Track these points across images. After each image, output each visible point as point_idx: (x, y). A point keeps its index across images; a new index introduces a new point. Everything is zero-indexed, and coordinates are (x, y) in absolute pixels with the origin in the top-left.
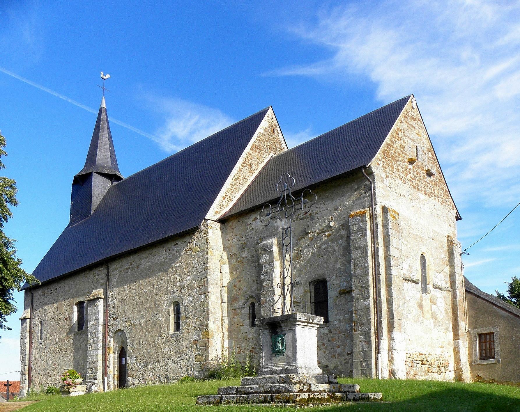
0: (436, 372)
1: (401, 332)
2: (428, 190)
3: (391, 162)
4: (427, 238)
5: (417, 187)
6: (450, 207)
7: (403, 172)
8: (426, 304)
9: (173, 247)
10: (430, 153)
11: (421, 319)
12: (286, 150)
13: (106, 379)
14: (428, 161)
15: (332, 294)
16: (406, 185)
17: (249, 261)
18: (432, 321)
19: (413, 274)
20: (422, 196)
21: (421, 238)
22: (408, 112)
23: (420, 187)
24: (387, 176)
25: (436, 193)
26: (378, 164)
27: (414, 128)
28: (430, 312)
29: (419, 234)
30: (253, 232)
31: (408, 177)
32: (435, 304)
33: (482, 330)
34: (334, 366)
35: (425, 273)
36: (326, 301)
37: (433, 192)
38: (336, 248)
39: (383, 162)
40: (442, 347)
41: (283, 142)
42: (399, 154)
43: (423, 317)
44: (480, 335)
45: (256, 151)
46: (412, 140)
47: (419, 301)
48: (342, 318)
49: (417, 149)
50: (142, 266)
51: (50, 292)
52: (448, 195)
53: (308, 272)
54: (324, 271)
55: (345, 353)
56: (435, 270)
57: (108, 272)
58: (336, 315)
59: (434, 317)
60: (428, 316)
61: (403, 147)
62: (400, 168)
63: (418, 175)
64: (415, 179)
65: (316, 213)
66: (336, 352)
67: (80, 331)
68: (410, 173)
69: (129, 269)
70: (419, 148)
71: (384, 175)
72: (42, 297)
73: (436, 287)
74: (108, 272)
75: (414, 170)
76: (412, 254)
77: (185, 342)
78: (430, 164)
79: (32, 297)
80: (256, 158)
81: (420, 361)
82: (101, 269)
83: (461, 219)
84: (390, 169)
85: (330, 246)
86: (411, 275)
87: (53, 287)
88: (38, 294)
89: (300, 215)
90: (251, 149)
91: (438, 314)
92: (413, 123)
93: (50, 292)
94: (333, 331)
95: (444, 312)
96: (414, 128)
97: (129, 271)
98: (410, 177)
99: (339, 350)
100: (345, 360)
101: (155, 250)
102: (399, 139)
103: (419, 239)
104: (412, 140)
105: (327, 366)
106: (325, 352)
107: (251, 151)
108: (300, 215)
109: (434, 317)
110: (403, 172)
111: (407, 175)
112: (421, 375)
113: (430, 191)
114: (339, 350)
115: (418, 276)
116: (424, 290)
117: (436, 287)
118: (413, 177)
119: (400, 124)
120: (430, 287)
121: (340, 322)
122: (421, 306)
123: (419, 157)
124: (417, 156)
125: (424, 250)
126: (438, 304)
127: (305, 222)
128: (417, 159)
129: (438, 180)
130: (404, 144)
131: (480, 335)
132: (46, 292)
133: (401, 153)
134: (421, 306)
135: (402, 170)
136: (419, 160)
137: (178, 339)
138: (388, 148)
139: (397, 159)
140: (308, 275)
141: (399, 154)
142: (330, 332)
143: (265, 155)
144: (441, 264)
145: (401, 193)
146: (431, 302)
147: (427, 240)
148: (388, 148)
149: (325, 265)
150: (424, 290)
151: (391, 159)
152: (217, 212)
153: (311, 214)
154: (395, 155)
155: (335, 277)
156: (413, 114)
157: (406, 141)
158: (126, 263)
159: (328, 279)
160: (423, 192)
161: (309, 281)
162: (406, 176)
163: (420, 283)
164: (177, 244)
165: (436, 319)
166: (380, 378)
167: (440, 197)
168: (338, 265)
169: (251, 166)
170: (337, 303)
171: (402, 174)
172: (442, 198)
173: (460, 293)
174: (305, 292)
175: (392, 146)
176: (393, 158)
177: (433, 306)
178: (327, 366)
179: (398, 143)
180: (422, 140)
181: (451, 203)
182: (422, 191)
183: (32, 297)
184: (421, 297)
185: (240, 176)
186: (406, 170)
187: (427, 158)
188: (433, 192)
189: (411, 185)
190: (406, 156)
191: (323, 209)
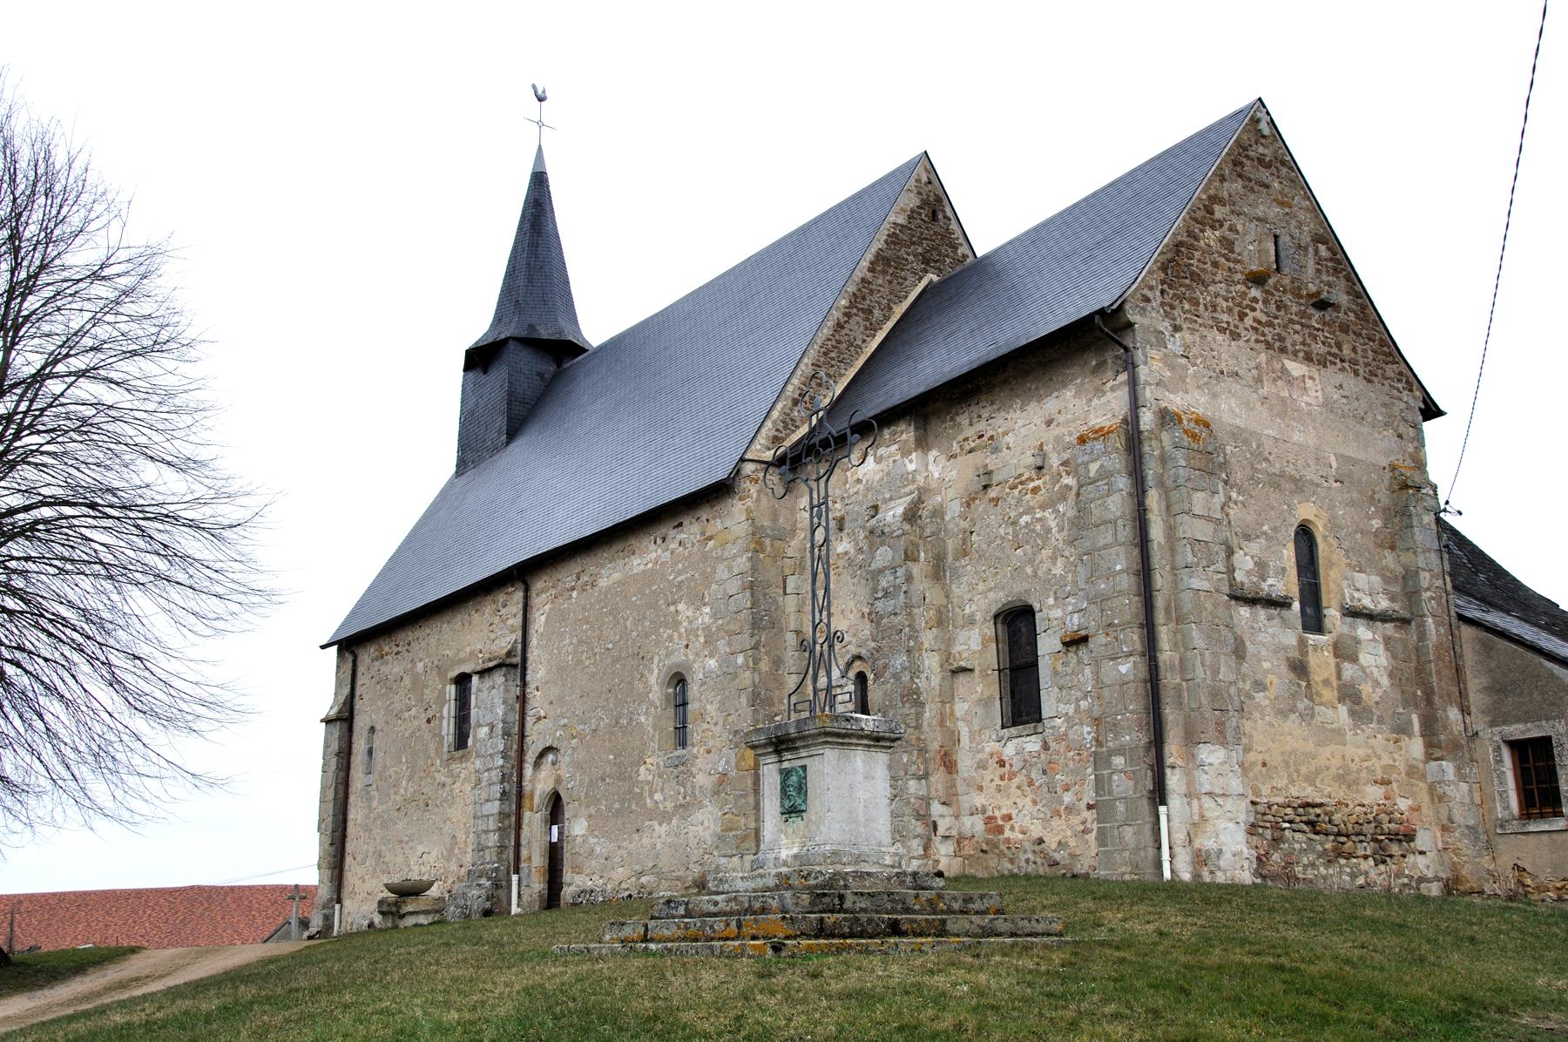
0: (1366, 857)
1: (1223, 743)
2: (1318, 348)
3: (1189, 287)
4: (1318, 480)
5: (1277, 344)
6: (1400, 386)
7: (1230, 310)
8: (1322, 662)
9: (672, 533)
10: (1322, 248)
11: (1302, 704)
12: (970, 259)
13: (1162, 809)
14: (1318, 271)
15: (1048, 645)
16: (1241, 343)
17: (851, 562)
18: (1343, 710)
19: (1270, 581)
20: (1296, 368)
21: (1293, 479)
22: (1245, 149)
23: (1288, 344)
24: (1177, 329)
25: (1347, 351)
26: (1147, 300)
27: (1268, 187)
28: (1335, 683)
29: (1290, 470)
30: (861, 487)
31: (1248, 321)
32: (1354, 659)
33: (1518, 731)
34: (1057, 839)
35: (1315, 574)
36: (1034, 665)
37: (1334, 350)
38: (1053, 524)
39: (1162, 292)
40: (1385, 782)
41: (961, 240)
42: (1215, 264)
43: (1312, 700)
44: (1514, 745)
45: (884, 272)
46: (1258, 219)
47: (1295, 654)
48: (1071, 709)
49: (1276, 244)
50: (603, 583)
51: (395, 649)
52: (1390, 354)
53: (990, 590)
54: (1026, 586)
55: (1083, 805)
56: (1349, 565)
57: (526, 598)
58: (1059, 701)
59: (1349, 694)
60: (1329, 694)
61: (1228, 244)
62: (1220, 300)
63: (1282, 313)
64: (1270, 324)
65: (1005, 433)
66: (1061, 802)
67: (461, 752)
68: (1254, 310)
69: (573, 589)
70: (1285, 240)
71: (1165, 326)
72: (377, 663)
73: (1353, 613)
74: (526, 598)
75: (1265, 302)
76: (1266, 528)
77: (701, 779)
78: (1325, 278)
79: (354, 662)
80: (885, 290)
81: (1306, 823)
82: (511, 589)
83: (1440, 413)
84: (1187, 306)
85: (1040, 520)
86: (1265, 586)
87: (409, 635)
88: (366, 655)
89: (966, 439)
90: (871, 270)
91: (1366, 689)
92: (1264, 175)
93: (395, 649)
94: (1053, 745)
95: (1385, 681)
96: (1268, 187)
97: (575, 594)
98: (1255, 320)
99: (1068, 798)
100: (1083, 823)
101: (633, 542)
102: (1216, 224)
103: (1287, 486)
104: (1258, 219)
105: (1041, 841)
106: (1035, 802)
107: (869, 275)
108: (966, 439)
109: (1349, 694)
110: (1230, 310)
111: (1242, 316)
112: (1313, 865)
113: (1323, 349)
114: (1068, 798)
115: (1284, 582)
116: (1314, 622)
117: (1353, 613)
118: (1264, 319)
119: (1217, 184)
120: (1332, 614)
121: (1068, 719)
122: (1300, 668)
123: (1285, 262)
124: (1277, 261)
125: (1306, 511)
126: (1365, 659)
127: (978, 458)
128: (1278, 270)
129: (1352, 316)
130: (1231, 236)
131: (1514, 745)
132: (387, 649)
133: (1223, 260)
134: (1300, 668)
135: (1224, 304)
136: (1286, 271)
137: (680, 769)
138: (1178, 252)
139: (1207, 278)
140: (991, 595)
141: (1215, 264)
142: (1046, 747)
143: (911, 279)
144: (1371, 547)
145: (1223, 366)
146: (1336, 655)
147: (1318, 485)
148: (1178, 252)
149: (1029, 570)
150: (1314, 622)
151: (1187, 281)
152: (776, 440)
153: (992, 438)
154: (1204, 270)
155: (1051, 601)
156: (1261, 150)
157: (1240, 228)
158: (567, 575)
159: (1036, 606)
160: (1301, 355)
161: (994, 611)
162: (1241, 319)
163: (1296, 606)
164: (681, 524)
165: (1358, 703)
166: (1167, 874)
167: (1361, 361)
168: (1058, 570)
169: (871, 312)
170: (1059, 668)
171: (1225, 317)
172: (1367, 365)
173: (1437, 625)
174: (984, 644)
175: (1191, 247)
176: (1195, 277)
177: (1346, 665)
178: (1041, 841)
179: (1211, 237)
180: (1295, 217)
181: (1401, 374)
182: (1295, 354)
183: (354, 662)
184: (1302, 643)
185: (839, 342)
186: (1239, 305)
187: (1311, 263)
188: (1334, 350)
189: (1257, 341)
190: (1238, 267)
191: (1020, 423)
